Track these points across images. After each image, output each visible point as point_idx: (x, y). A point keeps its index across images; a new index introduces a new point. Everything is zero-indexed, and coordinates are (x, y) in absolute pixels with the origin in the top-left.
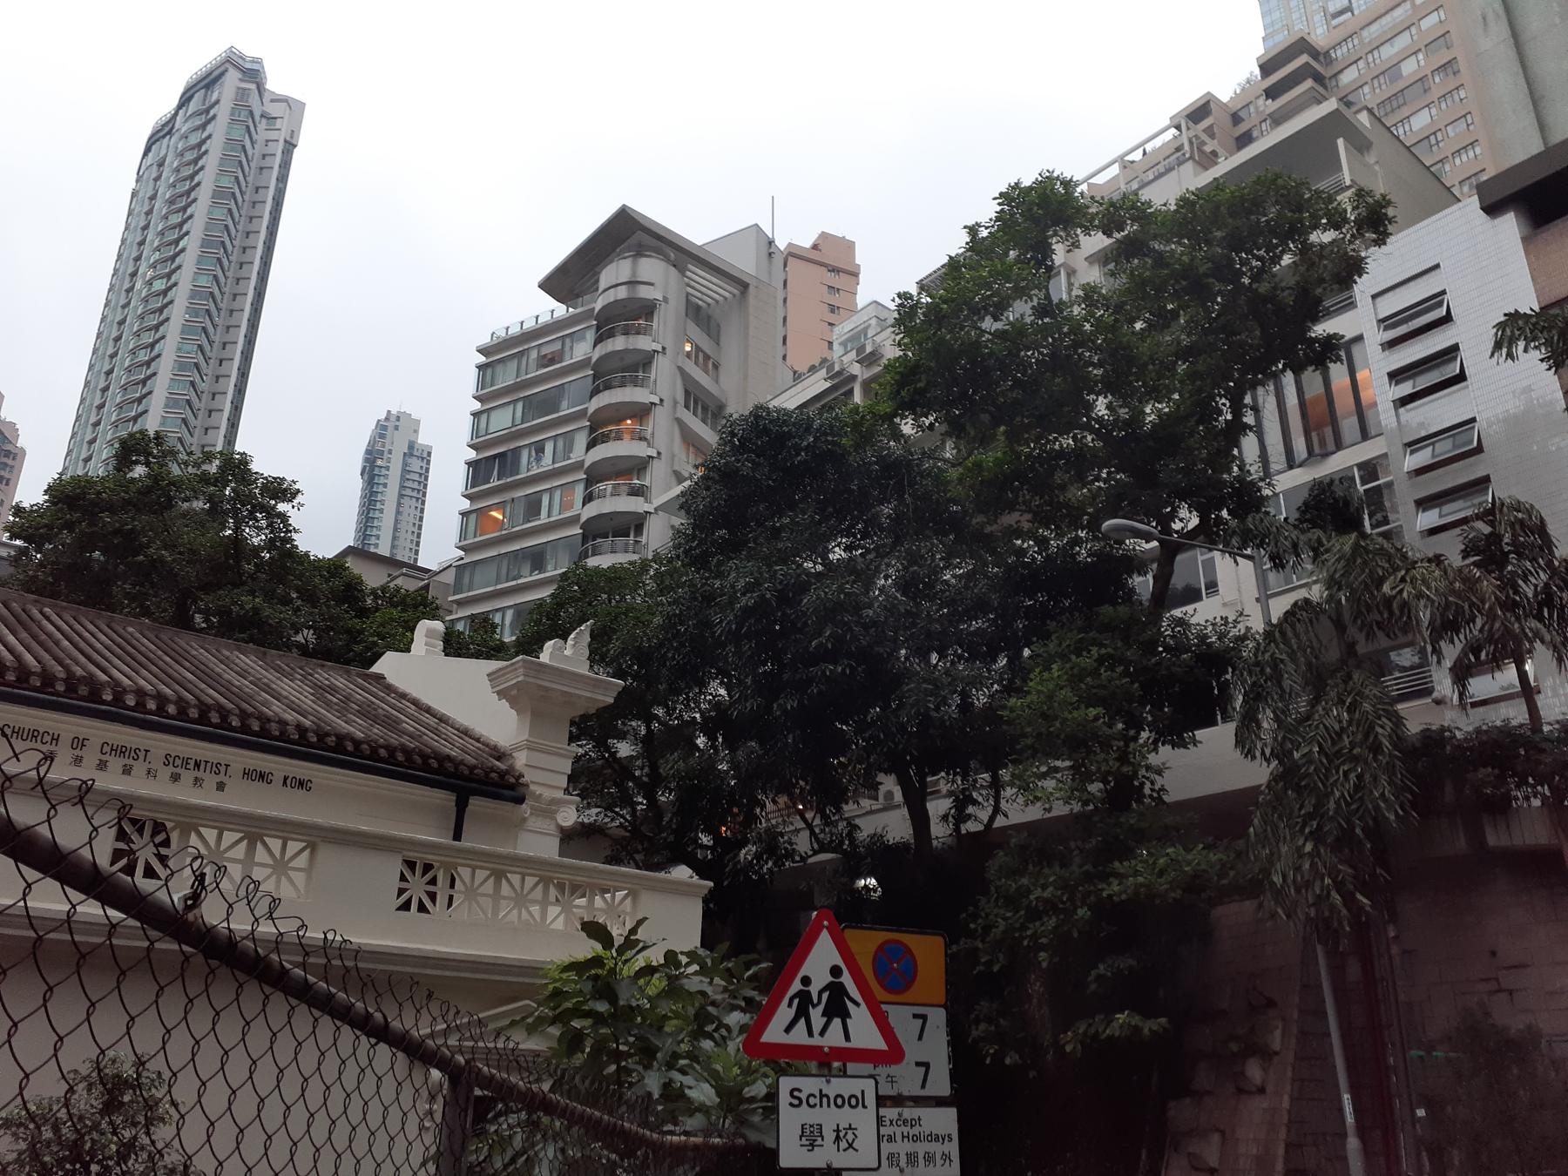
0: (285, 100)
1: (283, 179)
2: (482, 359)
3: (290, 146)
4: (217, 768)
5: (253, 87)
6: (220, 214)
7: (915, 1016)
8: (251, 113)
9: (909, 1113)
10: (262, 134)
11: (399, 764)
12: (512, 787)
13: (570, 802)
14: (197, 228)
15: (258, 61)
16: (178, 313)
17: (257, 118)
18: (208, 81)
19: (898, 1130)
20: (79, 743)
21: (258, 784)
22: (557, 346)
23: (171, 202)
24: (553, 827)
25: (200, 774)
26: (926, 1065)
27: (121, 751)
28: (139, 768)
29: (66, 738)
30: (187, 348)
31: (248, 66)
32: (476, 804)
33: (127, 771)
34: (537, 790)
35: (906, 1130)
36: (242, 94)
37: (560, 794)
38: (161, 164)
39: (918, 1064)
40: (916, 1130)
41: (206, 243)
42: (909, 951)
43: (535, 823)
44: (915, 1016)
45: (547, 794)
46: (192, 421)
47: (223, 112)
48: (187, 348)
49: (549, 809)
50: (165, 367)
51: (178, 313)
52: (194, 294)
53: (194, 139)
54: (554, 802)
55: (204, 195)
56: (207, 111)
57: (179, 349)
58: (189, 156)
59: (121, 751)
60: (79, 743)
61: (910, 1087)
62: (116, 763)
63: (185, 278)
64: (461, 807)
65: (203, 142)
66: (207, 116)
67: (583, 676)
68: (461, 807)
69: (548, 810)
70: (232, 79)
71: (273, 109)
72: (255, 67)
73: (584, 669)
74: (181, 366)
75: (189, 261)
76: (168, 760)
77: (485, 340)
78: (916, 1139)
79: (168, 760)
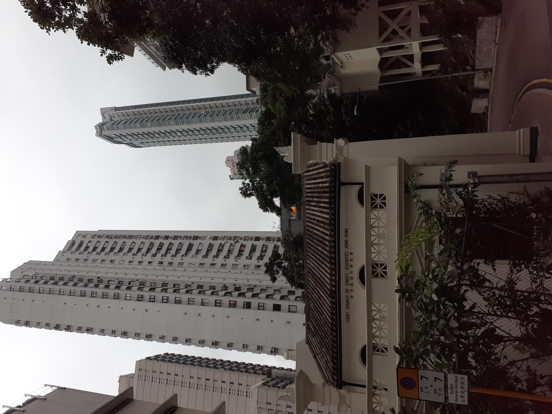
0: (103, 115)
1: (128, 108)
2: (167, 68)
3: (116, 109)
4: (346, 256)
5: (104, 126)
6: (149, 124)
7: (421, 379)
8: (113, 124)
9: (449, 386)
10: (116, 119)
11: (335, 206)
12: (335, 166)
13: (336, 142)
14: (157, 129)
15: (96, 127)
16: (186, 127)
17: (113, 122)
18: (110, 139)
19: (454, 390)
20: (347, 291)
21: (349, 232)
22: (152, 47)
23: (152, 138)
24: (346, 146)
25: (349, 260)
26: (435, 378)
27: (347, 281)
28: (350, 275)
29: (346, 294)
30: (194, 121)
31: (99, 130)
32: (343, 180)
33: (352, 278)
34: (334, 155)
35: (454, 388)
36: (108, 129)
37: (334, 145)
38: (143, 143)
39: (435, 381)
40: (455, 386)
41: (160, 125)
42: (402, 379)
43: (345, 153)
44: (421, 379)
45: (335, 152)
46: (216, 113)
47: (118, 132)
48: (194, 121)
49: (340, 149)
50: (203, 126)
51: (186, 127)
52: (177, 124)
53: (130, 137)
54: (337, 149)
55: (146, 130)
56: (119, 136)
57: (196, 123)
58: (136, 137)
59: (347, 281)
60: (347, 291)
61: (442, 385)
62: (350, 281)
63: (174, 128)
64: (344, 184)
65: (129, 135)
66: (121, 136)
67: (294, 147)
68: (344, 184)
69: (340, 149)
70: (105, 133)
71: (108, 118)
72: (98, 127)
73: (291, 148)
74: (201, 121)
75: (168, 128)
76: (347, 268)
77: (159, 69)
78: (457, 386)
79: (347, 268)
